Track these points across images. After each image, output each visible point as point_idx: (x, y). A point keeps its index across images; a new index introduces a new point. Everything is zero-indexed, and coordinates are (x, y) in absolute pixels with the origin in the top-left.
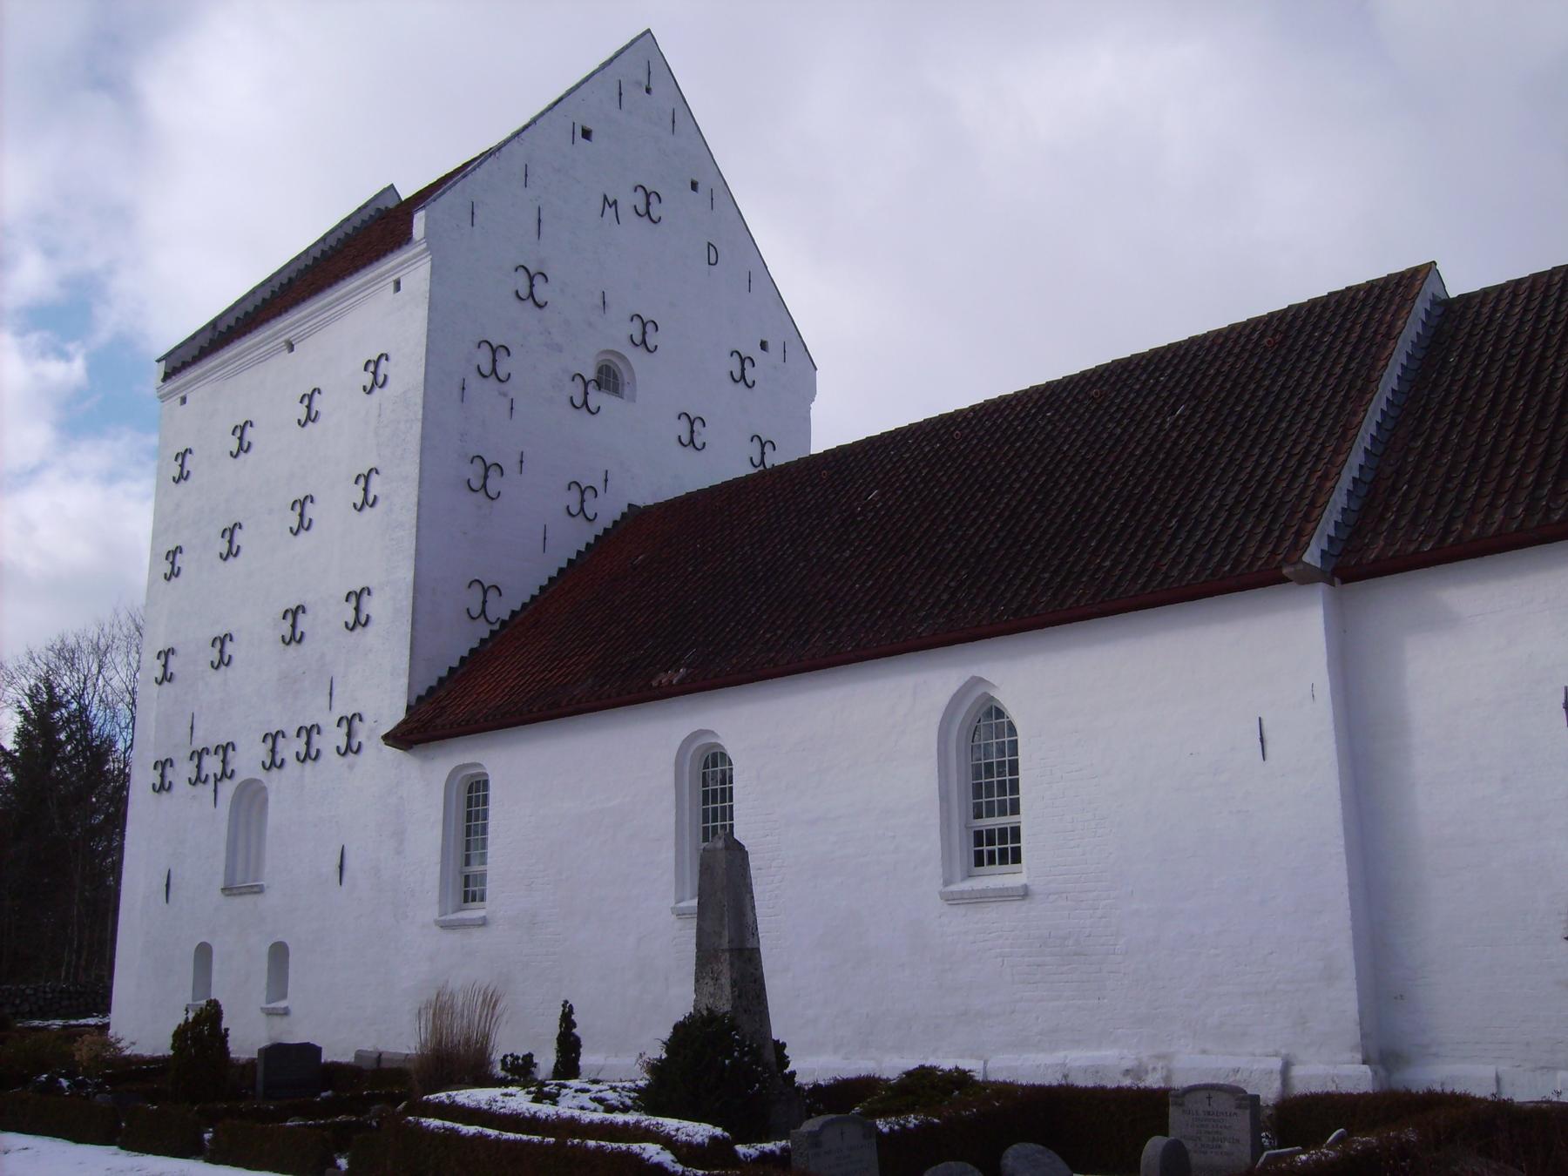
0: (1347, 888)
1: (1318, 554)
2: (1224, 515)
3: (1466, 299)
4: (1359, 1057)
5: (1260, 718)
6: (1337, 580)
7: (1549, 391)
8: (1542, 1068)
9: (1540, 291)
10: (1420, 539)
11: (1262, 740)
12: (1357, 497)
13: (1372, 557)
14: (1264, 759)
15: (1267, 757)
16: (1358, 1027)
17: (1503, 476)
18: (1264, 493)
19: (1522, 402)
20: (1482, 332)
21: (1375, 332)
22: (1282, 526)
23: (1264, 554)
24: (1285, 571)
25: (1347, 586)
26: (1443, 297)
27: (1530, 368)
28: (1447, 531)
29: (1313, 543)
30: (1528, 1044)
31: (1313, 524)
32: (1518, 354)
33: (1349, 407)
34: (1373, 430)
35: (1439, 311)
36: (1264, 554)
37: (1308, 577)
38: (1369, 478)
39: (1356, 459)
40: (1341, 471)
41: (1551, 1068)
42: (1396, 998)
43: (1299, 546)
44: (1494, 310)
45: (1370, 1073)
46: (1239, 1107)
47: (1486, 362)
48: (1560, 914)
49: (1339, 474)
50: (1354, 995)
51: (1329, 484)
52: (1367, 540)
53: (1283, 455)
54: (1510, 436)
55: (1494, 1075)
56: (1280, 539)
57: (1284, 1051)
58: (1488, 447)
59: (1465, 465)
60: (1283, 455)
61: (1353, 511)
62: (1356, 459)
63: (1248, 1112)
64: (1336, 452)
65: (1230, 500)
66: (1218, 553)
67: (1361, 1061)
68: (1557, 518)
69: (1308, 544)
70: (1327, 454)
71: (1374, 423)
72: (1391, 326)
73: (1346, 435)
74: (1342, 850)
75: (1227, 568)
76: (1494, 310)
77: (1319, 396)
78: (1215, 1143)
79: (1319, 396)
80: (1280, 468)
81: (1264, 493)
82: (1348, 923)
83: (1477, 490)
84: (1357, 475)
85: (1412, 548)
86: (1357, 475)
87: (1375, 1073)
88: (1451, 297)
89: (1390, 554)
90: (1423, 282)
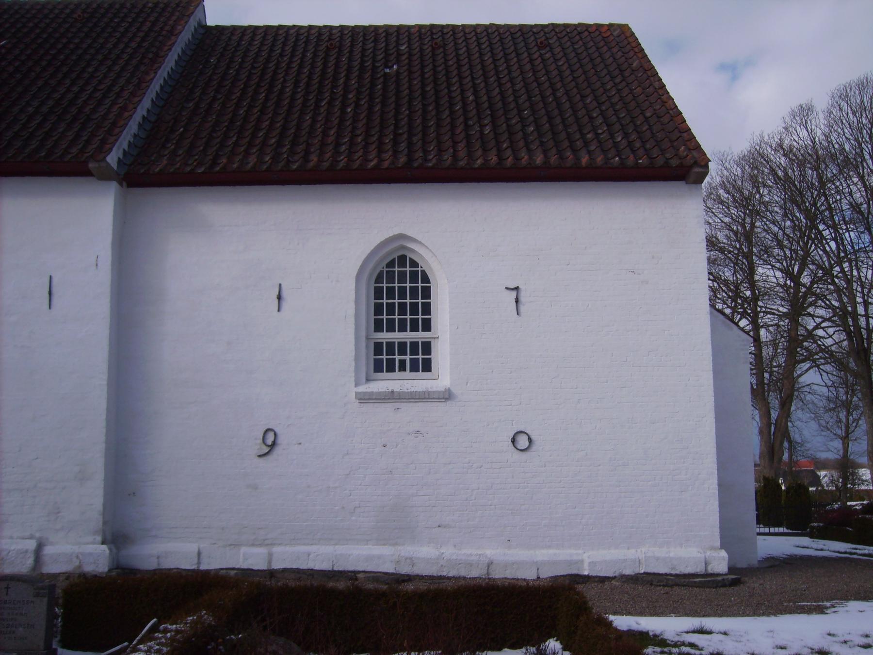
0: (105, 412)
1: (116, 159)
2: (39, 119)
3: (220, 30)
4: (99, 538)
5: (51, 277)
6: (125, 184)
7: (282, 92)
8: (231, 545)
9: (271, 36)
10: (195, 164)
11: (50, 293)
12: (145, 130)
13: (158, 169)
14: (50, 308)
15: (52, 306)
16: (102, 517)
17: (254, 136)
18: (74, 110)
19: (264, 94)
20: (233, 49)
21: (162, 29)
22: (89, 134)
23: (74, 150)
24: (91, 165)
25: (130, 189)
26: (204, 24)
27: (268, 76)
28: (214, 162)
29: (115, 149)
30: (223, 529)
31: (115, 138)
32: (259, 67)
33: (143, 68)
34: (158, 88)
35: (202, 31)
36: (74, 150)
37: (105, 176)
38: (153, 119)
39: (146, 104)
40: (137, 107)
41: (237, 545)
42: (129, 495)
43: (104, 148)
44: (241, 39)
45: (107, 551)
46: (37, 595)
47: (237, 67)
48: (256, 439)
49: (135, 108)
50: (100, 492)
51: (126, 114)
52: (153, 158)
53: (90, 89)
54: (257, 113)
55: (196, 551)
56: (88, 142)
57: (37, 535)
58: (261, 101)
59: (226, 124)
60: (90, 89)
61: (141, 138)
62: (146, 104)
63: (45, 600)
64: (133, 94)
65: (45, 109)
66: (34, 144)
67: (100, 542)
68: (295, 167)
69: (111, 150)
70: (126, 94)
71: (159, 84)
72: (173, 28)
73: (141, 86)
74: (105, 383)
75: (43, 154)
76: (241, 39)
77: (119, 57)
78: (9, 629)
79: (119, 57)
80: (87, 96)
81: (74, 110)
82: (103, 438)
83: (236, 141)
84: (145, 114)
85: (188, 169)
86: (145, 114)
87: (110, 549)
88: (208, 25)
89: (172, 170)
90: (196, 8)
